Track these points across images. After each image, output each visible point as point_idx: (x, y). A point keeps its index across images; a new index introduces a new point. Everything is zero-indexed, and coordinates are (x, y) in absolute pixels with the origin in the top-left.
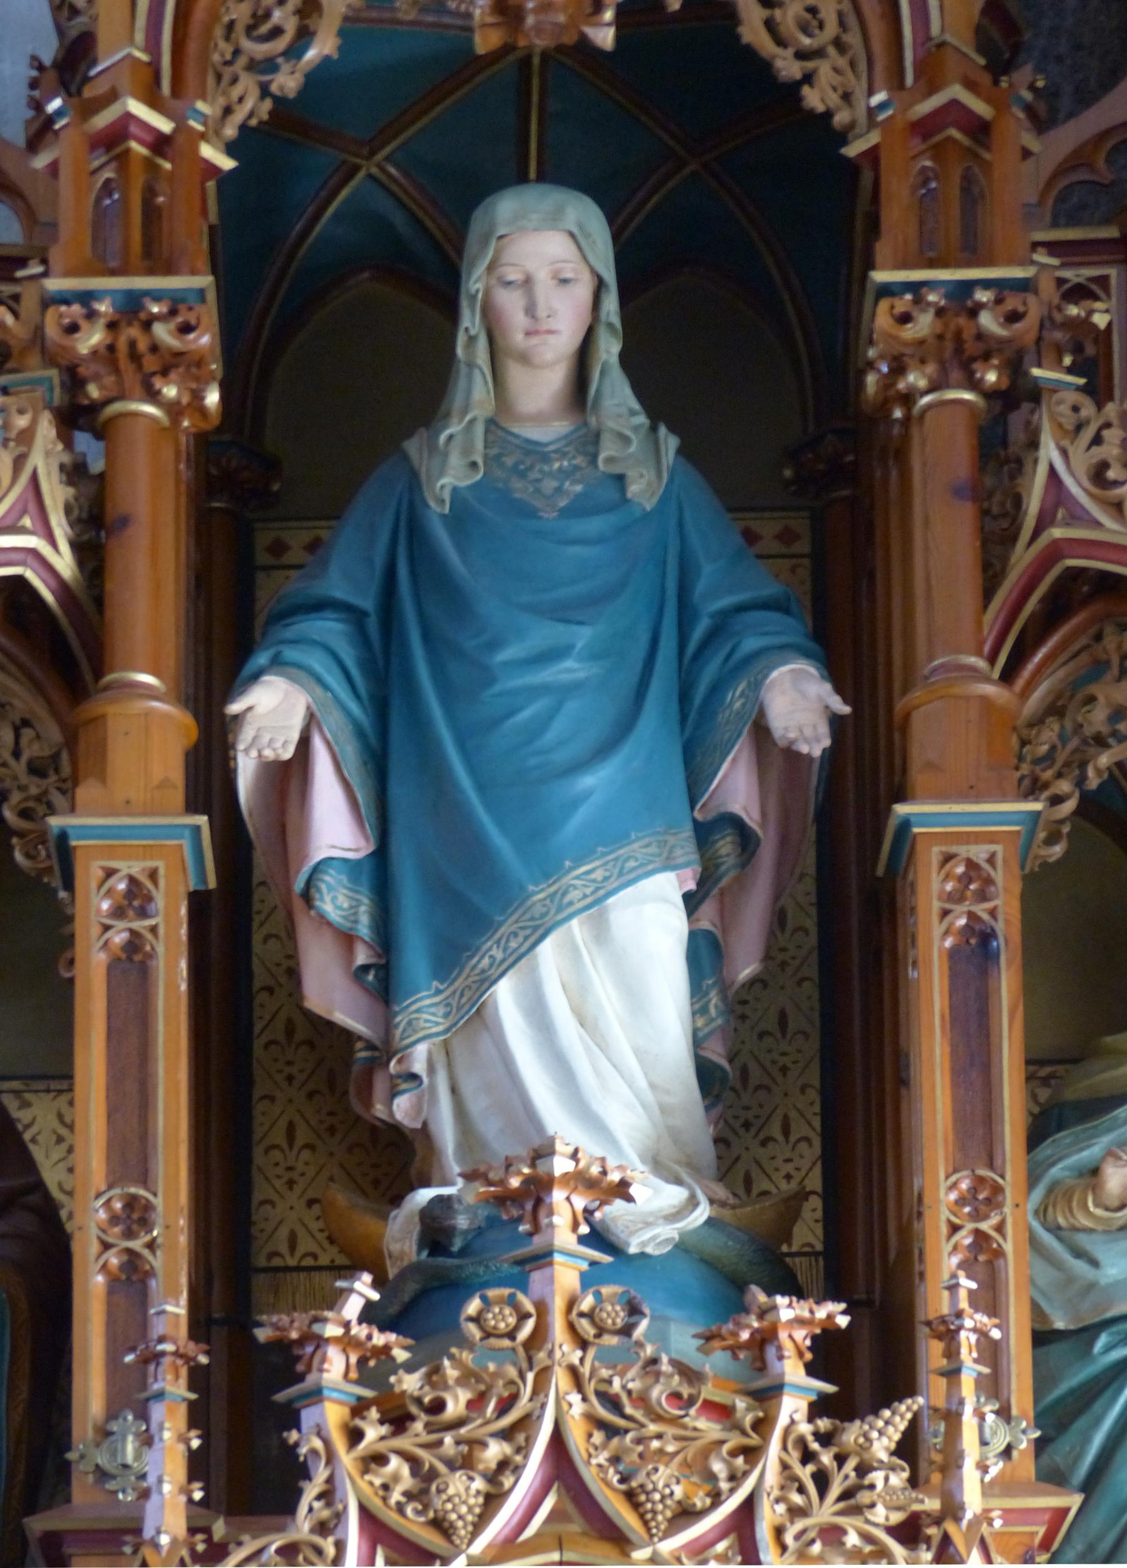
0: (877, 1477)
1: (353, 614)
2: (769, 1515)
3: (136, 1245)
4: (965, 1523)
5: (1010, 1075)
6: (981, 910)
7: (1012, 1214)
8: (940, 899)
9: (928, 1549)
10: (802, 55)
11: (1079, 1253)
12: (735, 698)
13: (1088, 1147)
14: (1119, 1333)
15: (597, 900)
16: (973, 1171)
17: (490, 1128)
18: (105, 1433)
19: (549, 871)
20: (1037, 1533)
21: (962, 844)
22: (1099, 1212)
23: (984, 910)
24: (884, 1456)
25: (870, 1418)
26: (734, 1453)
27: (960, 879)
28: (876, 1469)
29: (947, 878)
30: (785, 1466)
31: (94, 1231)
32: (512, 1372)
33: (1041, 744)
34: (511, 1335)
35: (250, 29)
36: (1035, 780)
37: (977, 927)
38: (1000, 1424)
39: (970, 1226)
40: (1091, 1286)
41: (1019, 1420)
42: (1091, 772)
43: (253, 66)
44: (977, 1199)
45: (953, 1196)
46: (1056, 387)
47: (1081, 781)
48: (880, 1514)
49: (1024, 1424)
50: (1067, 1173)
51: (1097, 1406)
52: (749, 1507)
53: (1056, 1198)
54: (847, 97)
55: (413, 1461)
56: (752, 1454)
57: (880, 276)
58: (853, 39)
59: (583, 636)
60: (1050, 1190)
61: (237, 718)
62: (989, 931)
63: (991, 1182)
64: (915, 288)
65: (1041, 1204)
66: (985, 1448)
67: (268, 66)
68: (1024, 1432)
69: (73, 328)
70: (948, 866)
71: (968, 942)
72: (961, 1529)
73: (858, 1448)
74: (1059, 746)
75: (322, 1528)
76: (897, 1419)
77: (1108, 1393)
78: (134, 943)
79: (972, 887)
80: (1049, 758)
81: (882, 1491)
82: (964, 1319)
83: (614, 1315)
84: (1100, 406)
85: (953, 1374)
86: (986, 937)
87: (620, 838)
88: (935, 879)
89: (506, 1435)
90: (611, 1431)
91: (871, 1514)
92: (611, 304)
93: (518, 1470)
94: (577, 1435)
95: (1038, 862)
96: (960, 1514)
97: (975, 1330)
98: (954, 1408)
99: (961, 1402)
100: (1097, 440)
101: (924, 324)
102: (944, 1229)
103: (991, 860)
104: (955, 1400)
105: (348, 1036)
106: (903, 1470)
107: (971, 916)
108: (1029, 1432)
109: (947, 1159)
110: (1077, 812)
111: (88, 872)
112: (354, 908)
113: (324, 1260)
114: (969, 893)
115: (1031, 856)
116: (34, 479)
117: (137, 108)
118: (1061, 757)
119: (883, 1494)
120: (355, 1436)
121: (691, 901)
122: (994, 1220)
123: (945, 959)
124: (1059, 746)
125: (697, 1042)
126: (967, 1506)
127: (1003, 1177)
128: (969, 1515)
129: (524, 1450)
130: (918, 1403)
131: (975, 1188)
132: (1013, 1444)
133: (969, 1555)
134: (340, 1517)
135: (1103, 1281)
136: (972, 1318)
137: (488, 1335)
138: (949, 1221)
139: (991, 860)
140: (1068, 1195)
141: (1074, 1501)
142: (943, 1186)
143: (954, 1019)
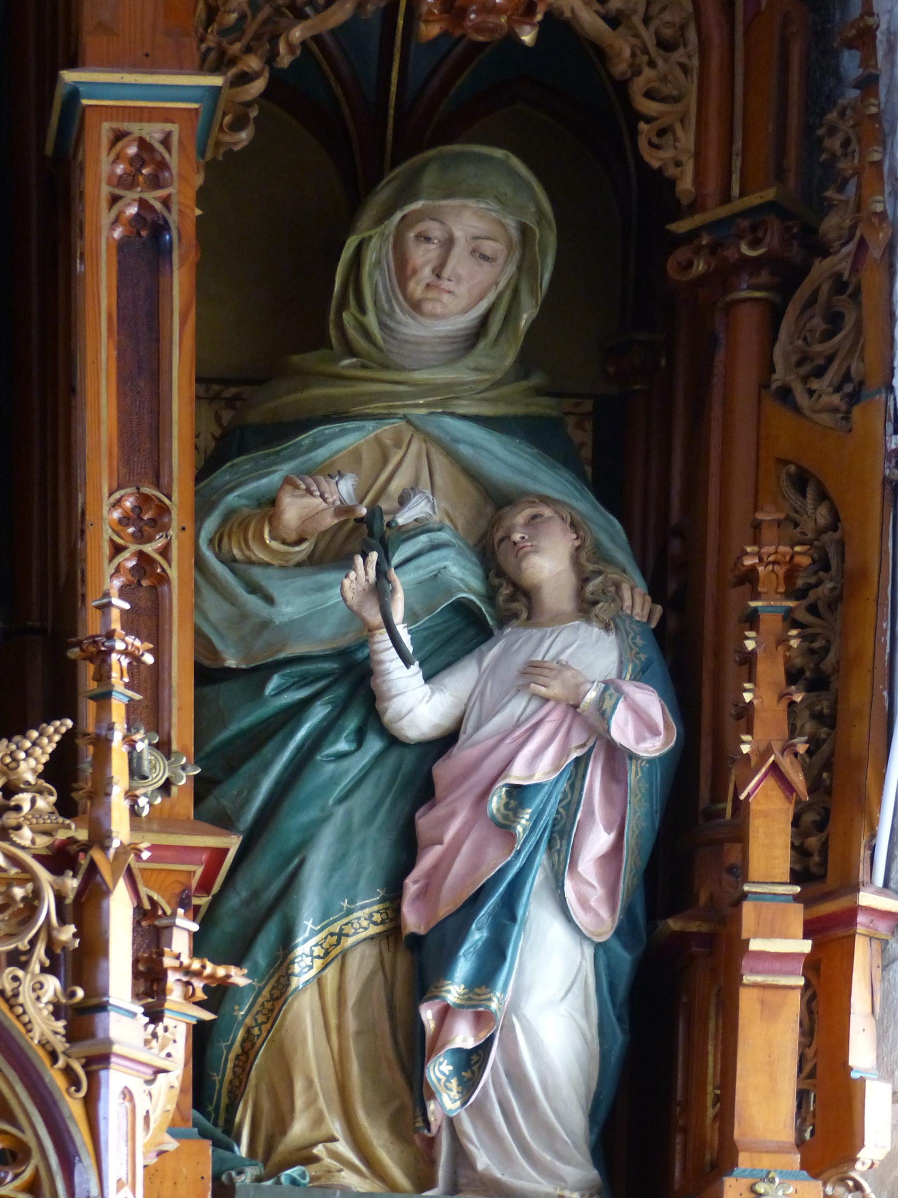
0: (24, 799)
3: (149, 549)
4: (112, 852)
5: (180, 387)
6: (153, 197)
7: (178, 537)
8: (109, 183)
9: (74, 876)
11: (254, 589)
13: (267, 474)
14: (290, 675)
16: (138, 489)
20: (194, 872)
21: (135, 121)
22: (275, 545)
23: (156, 198)
24: (31, 778)
25: (17, 738)
27: (131, 161)
28: (23, 791)
29: (117, 159)
33: (230, 12)
36: (222, 53)
37: (149, 218)
38: (159, 757)
39: (133, 548)
40: (265, 624)
41: (179, 754)
42: (282, 48)
44: (142, 520)
45: (116, 515)
47: (271, 58)
48: (26, 835)
49: (184, 760)
50: (244, 502)
51: (267, 751)
53: (231, 529)
60: (226, 519)
62: (161, 222)
63: (157, 502)
65: (216, 533)
66: (138, 782)
68: (183, 768)
70: (120, 145)
71: (139, 234)
72: (108, 859)
73: (5, 768)
74: (249, 14)
76: (45, 740)
77: (279, 737)
79: (144, 171)
80: (237, 29)
81: (27, 814)
82: (114, 641)
85: (104, 697)
86: (159, 228)
88: (105, 160)
91: (17, 836)
95: (222, 150)
96: (107, 843)
97: (125, 653)
98: (104, 732)
99: (111, 728)
102: (107, 550)
104: (105, 726)
106: (51, 794)
107: (143, 204)
108: (189, 769)
109: (111, 474)
110: (265, 94)
114: (141, 178)
115: (211, 142)
118: (252, 28)
119: (30, 817)
122: (159, 543)
123: (114, 251)
124: (249, 14)
126: (114, 835)
127: (170, 498)
128: (116, 844)
130: (66, 725)
131: (140, 508)
132: (173, 780)
133: (115, 885)
135: (278, 620)
136: (123, 640)
138: (111, 541)
139: (166, 141)
140: (244, 526)
141: (233, 843)
142: (106, 503)
143: (121, 320)
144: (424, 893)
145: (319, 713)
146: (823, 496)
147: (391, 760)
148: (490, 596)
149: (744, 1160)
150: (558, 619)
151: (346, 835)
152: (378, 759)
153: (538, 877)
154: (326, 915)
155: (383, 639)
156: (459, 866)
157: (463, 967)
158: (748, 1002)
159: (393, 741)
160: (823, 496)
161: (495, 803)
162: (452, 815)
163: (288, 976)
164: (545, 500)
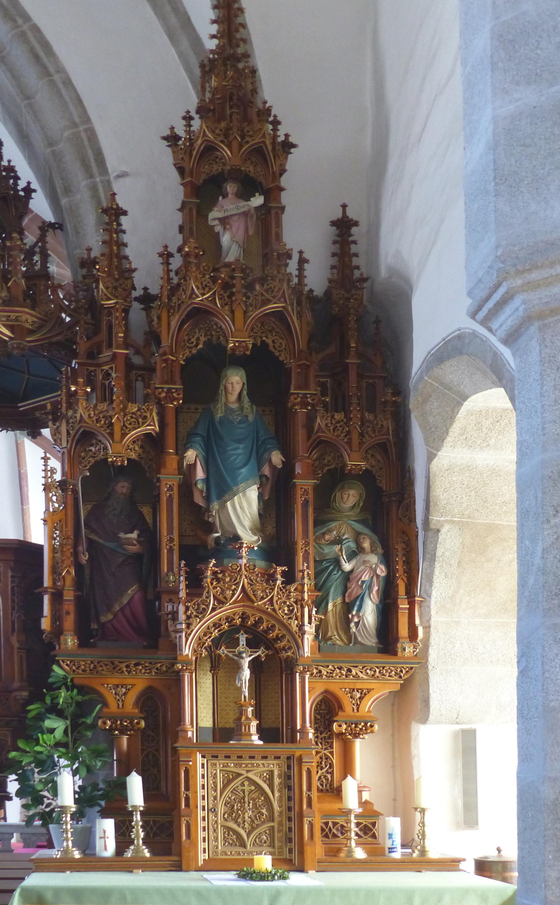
1: (203, 437)
2: (275, 599)
6: (306, 497)
10: (279, 351)
11: (321, 548)
12: (266, 455)
15: (244, 491)
17: (225, 523)
18: (167, 575)
19: (236, 484)
26: (270, 589)
30: (278, 591)
31: (165, 542)
32: (236, 575)
34: (236, 569)
35: (188, 341)
40: (322, 553)
43: (188, 347)
46: (320, 410)
52: (272, 597)
54: (286, 358)
55: (221, 588)
56: (273, 589)
57: (292, 392)
58: (287, 348)
59: (242, 446)
61: (185, 457)
64: (298, 394)
67: (191, 348)
69: (160, 393)
75: (207, 597)
78: (171, 495)
83: (252, 567)
84: (327, 413)
87: (247, 480)
88: (300, 492)
89: (235, 585)
90: (251, 585)
92: (245, 387)
93: (237, 590)
94: (246, 585)
100: (326, 419)
101: (299, 400)
103: (308, 489)
105: (201, 507)
110: (321, 477)
111: (163, 483)
112: (203, 487)
113: (191, 534)
116: (153, 417)
117: (170, 357)
120: (212, 584)
121: (258, 488)
125: (259, 510)
129: (238, 587)
134: (210, 596)
137: (232, 569)
144: (349, 596)
145: (331, 567)
146: (407, 535)
147: (343, 575)
148: (357, 548)
149: (400, 640)
150: (368, 553)
151: (336, 587)
152: (341, 574)
153: (367, 594)
154: (333, 599)
155: (341, 557)
156: (354, 592)
157: (356, 609)
158: (399, 614)
159: (343, 572)
160: (407, 535)
161: (360, 583)
162: (353, 584)
163: (327, 609)
164: (365, 534)
